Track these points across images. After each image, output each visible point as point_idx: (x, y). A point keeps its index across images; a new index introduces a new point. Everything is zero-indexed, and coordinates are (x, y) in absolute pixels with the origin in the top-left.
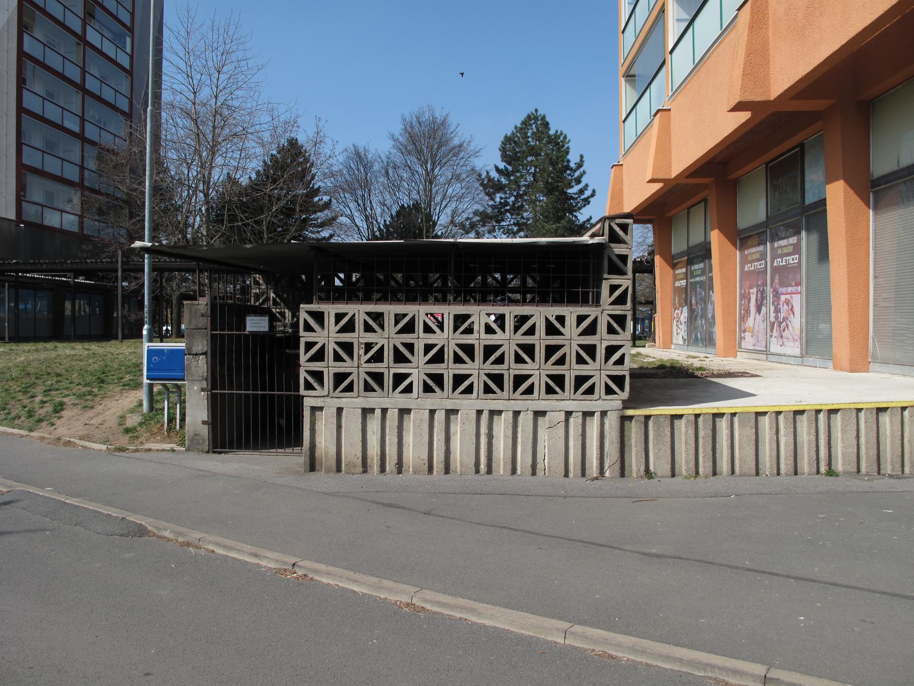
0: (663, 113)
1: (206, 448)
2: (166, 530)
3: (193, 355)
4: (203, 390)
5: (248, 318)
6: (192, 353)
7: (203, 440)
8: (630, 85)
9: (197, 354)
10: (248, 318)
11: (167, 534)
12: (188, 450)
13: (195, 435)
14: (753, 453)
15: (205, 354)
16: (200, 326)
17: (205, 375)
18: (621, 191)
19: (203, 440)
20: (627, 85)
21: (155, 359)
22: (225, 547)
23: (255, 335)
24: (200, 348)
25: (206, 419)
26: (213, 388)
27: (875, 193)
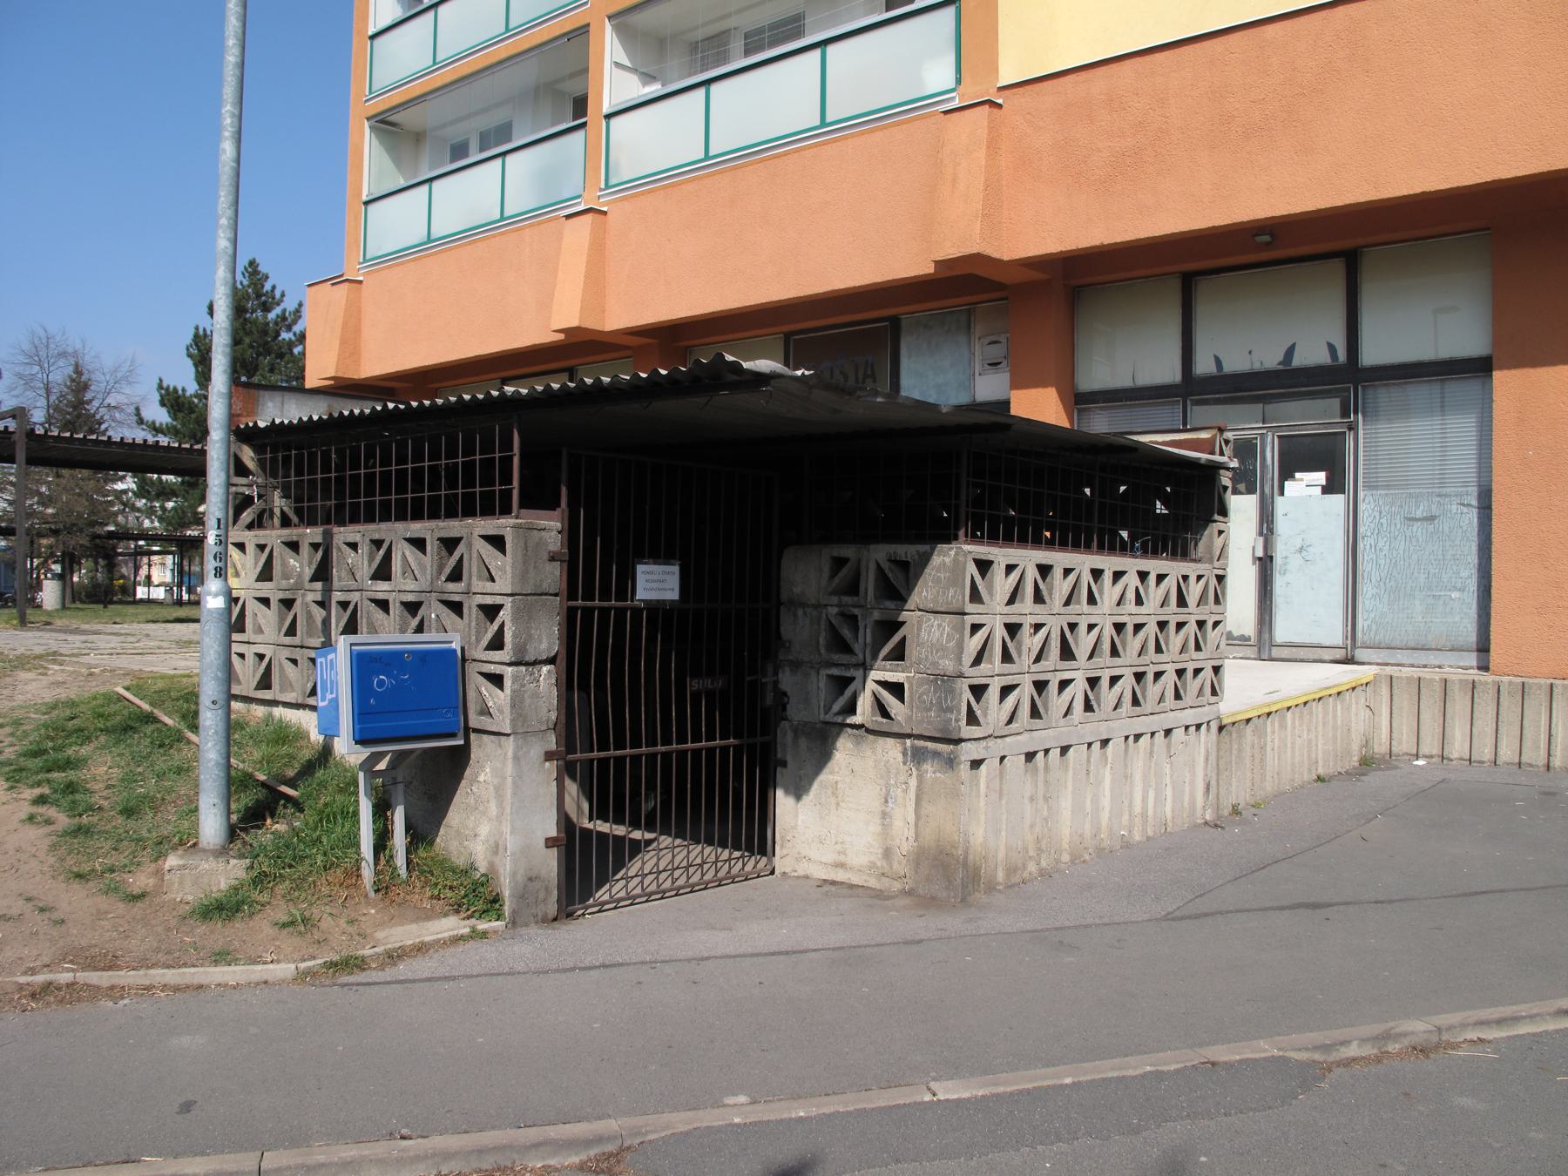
0: (597, 216)
1: (552, 909)
2: (1345, 1043)
3: (527, 664)
4: (549, 756)
5: (640, 568)
6: (527, 659)
7: (547, 889)
8: (375, 134)
9: (535, 663)
10: (640, 568)
11: (1353, 1051)
12: (513, 923)
13: (530, 879)
14: (1473, 741)
15: (551, 661)
16: (545, 587)
17: (554, 716)
18: (357, 330)
19: (547, 889)
20: (372, 134)
21: (381, 683)
22: (1500, 1022)
23: (654, 608)
24: (544, 646)
25: (554, 834)
26: (571, 749)
27: (1079, 410)
